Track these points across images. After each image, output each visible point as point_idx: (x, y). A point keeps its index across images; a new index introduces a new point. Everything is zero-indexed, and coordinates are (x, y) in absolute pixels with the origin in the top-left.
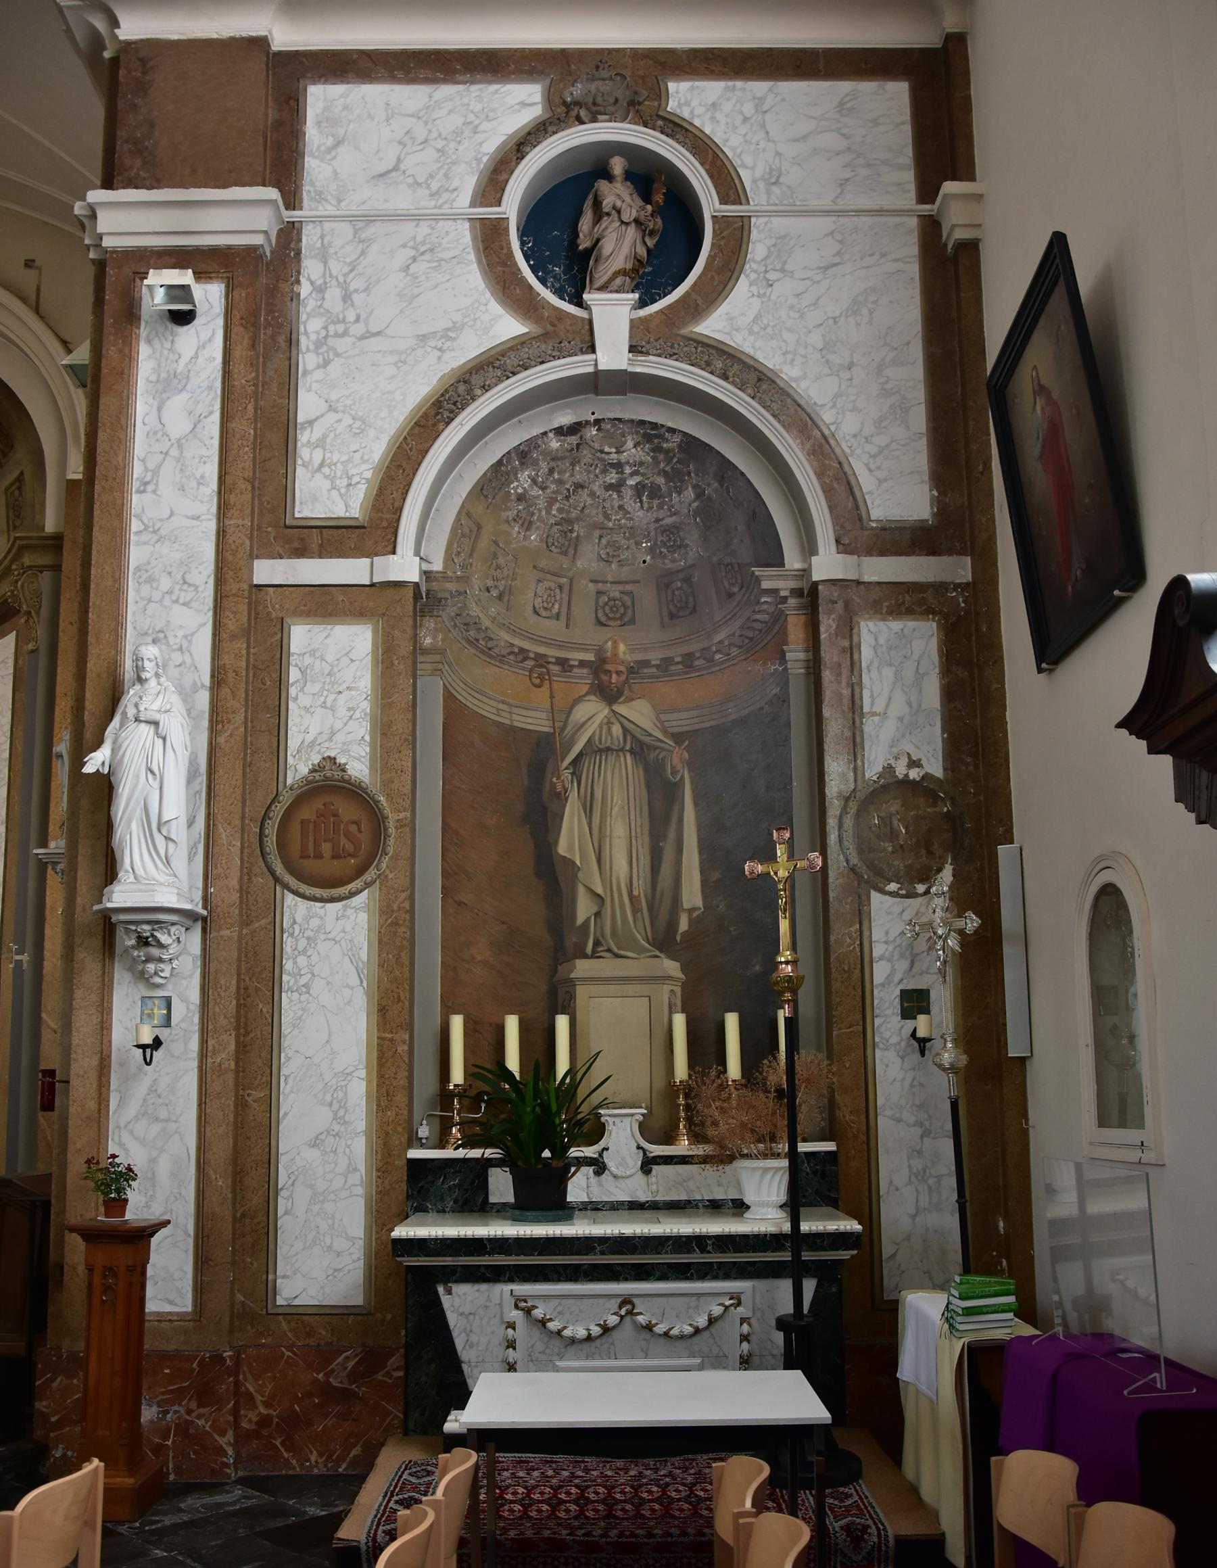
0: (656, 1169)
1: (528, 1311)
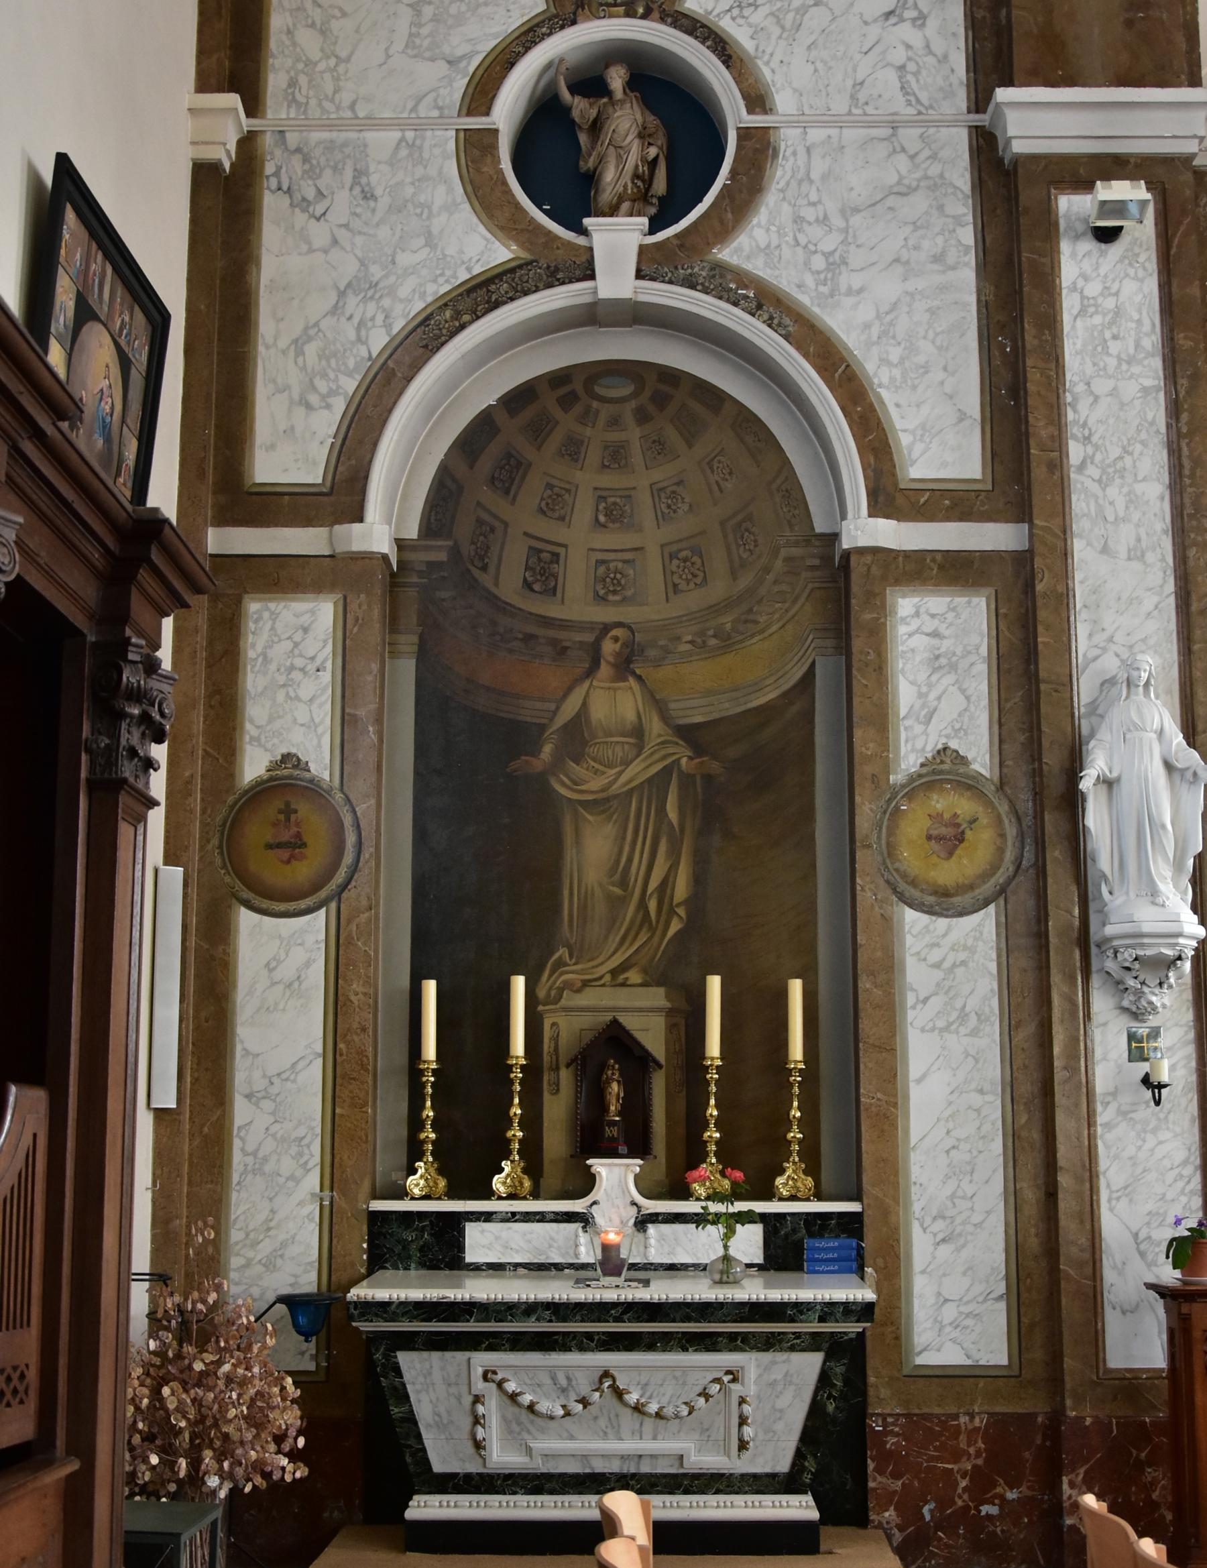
0: (652, 1229)
1: (500, 1385)
